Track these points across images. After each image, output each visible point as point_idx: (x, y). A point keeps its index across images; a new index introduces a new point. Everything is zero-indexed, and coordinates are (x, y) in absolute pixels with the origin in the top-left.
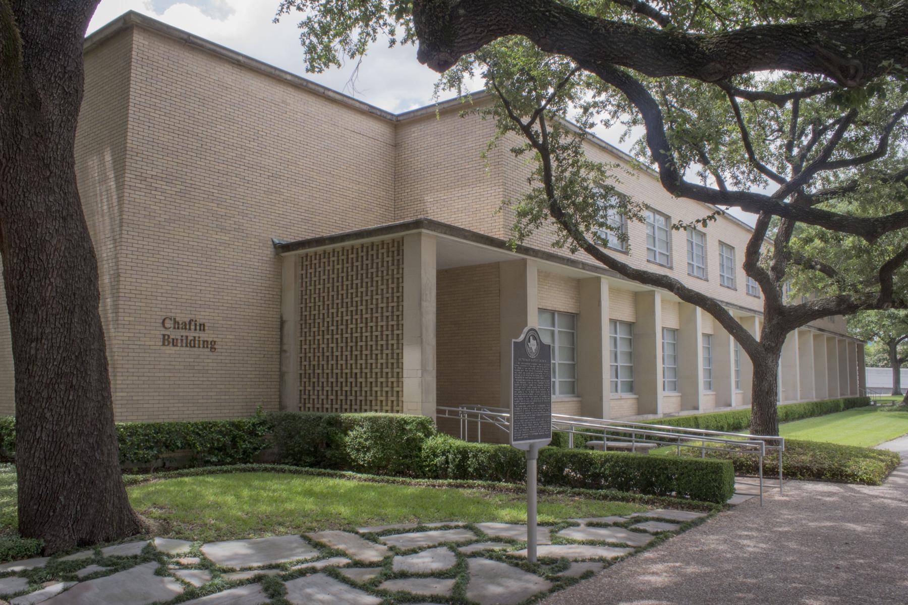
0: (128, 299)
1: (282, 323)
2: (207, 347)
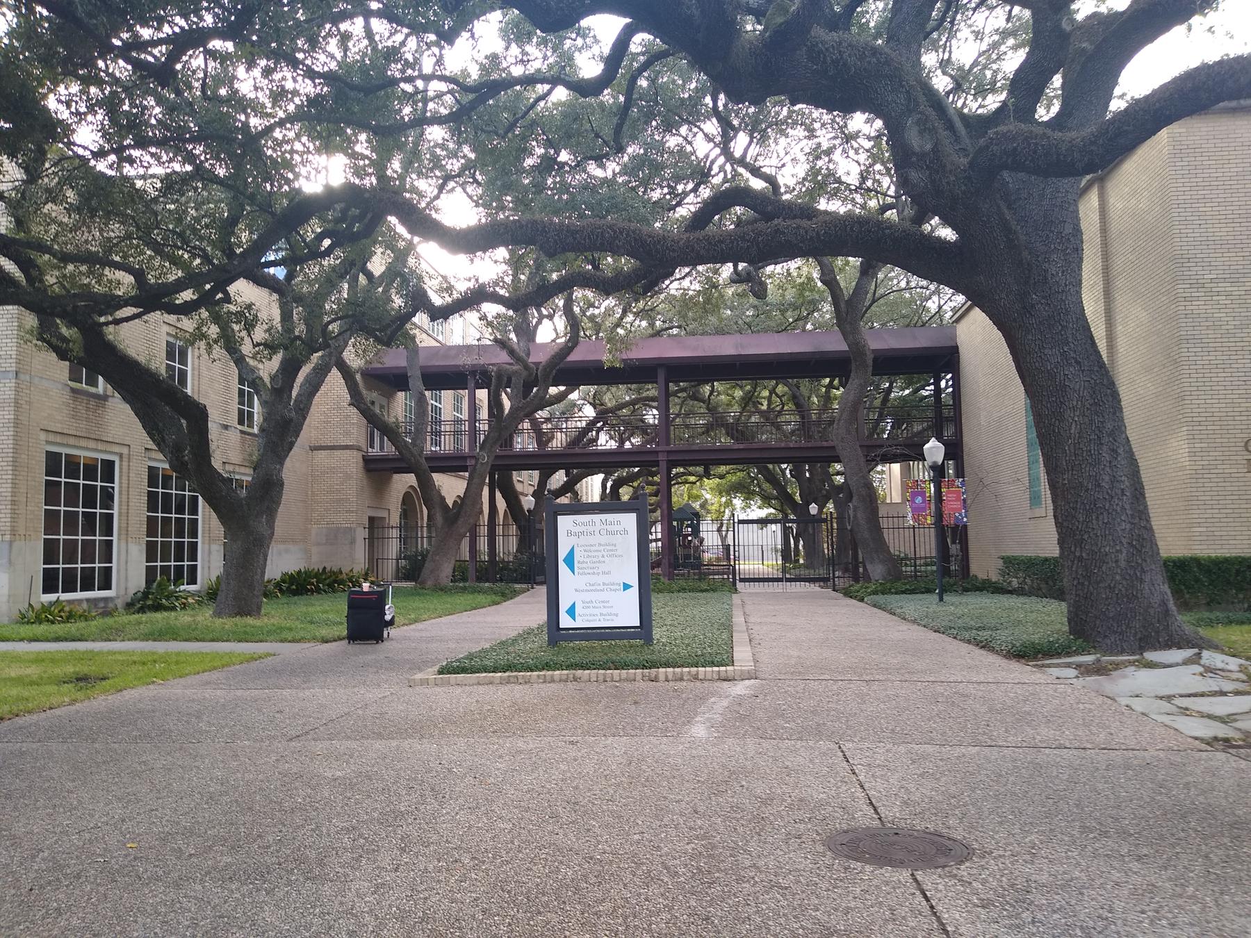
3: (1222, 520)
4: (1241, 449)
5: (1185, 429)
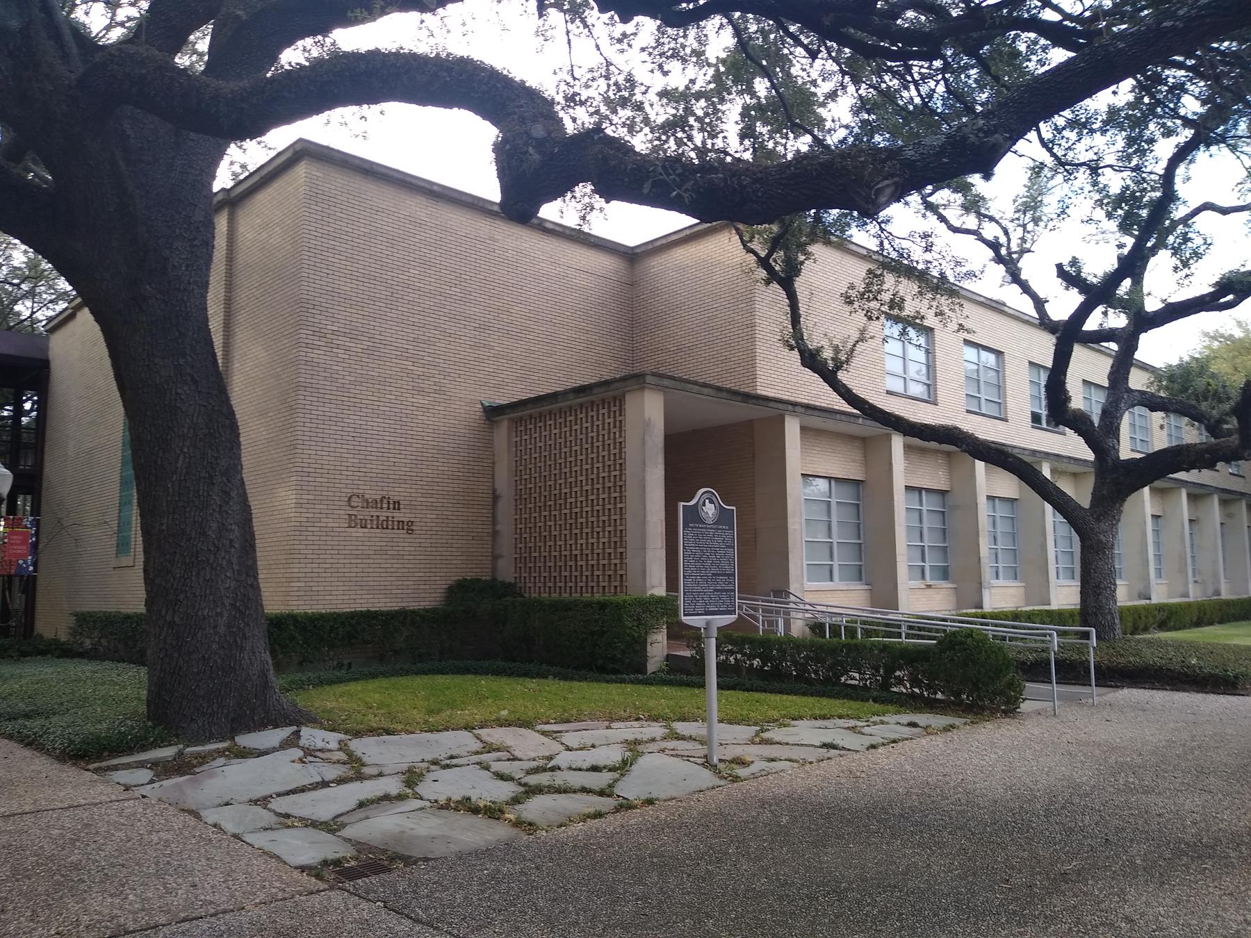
0: (306, 474)
1: (495, 498)
2: (403, 529)
3: (321, 575)
4: (344, 503)
5: (294, 478)
